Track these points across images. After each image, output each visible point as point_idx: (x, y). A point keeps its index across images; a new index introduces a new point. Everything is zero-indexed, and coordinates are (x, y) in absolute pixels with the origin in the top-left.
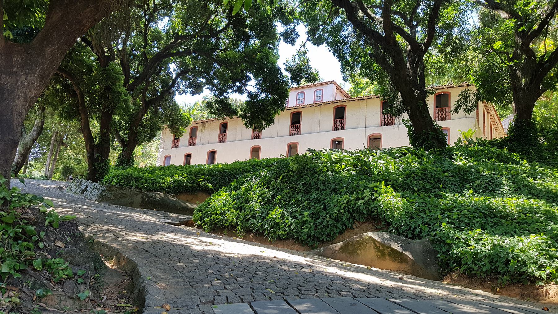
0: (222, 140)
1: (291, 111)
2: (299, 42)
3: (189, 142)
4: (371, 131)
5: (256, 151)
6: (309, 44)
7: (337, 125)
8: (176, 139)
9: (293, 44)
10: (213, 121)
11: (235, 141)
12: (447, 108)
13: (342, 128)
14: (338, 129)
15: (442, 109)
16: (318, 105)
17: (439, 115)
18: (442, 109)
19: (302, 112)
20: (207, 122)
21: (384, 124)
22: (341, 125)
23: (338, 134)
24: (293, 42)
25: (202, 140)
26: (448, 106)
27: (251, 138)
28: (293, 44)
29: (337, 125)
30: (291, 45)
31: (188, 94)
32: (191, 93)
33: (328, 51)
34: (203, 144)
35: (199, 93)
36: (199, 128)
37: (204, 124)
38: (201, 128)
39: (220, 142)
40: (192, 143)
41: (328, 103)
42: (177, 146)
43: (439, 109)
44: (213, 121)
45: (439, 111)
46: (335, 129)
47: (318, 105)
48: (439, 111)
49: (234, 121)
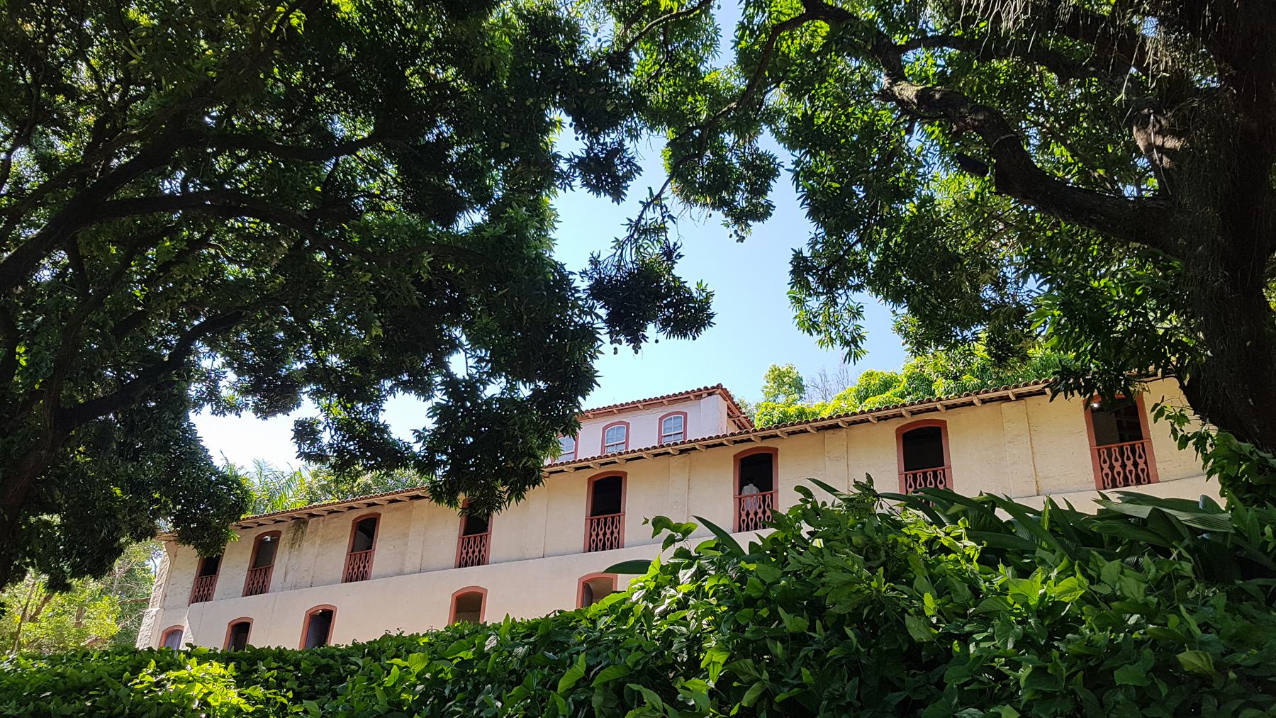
0: (357, 571)
1: (590, 473)
2: (637, 190)
3: (247, 584)
4: (316, 599)
5: (469, 604)
6: (673, 202)
7: (597, 535)
8: (209, 569)
9: (617, 195)
10: (331, 512)
11: (401, 573)
12: (1138, 444)
13: (480, 561)
14: (354, 577)
15: (925, 474)
16: (682, 452)
17: (1112, 468)
18: (925, 474)
19: (625, 474)
20: (311, 515)
21: (1114, 479)
22: (612, 533)
23: (471, 578)
24: (615, 187)
25: (289, 577)
26: (486, 530)
27: (453, 562)
28: (617, 195)
29: (597, 535)
30: (609, 199)
31: (248, 415)
32: (257, 410)
33: (735, 237)
34: (294, 587)
35: (286, 410)
36: (283, 536)
37: (300, 521)
38: (290, 535)
39: (350, 577)
40: (257, 583)
41: (713, 444)
42: (363, 576)
43: (915, 475)
44: (331, 512)
45: (1110, 456)
46: (463, 563)
47: (682, 452)
48: (1110, 456)
49: (397, 509)
